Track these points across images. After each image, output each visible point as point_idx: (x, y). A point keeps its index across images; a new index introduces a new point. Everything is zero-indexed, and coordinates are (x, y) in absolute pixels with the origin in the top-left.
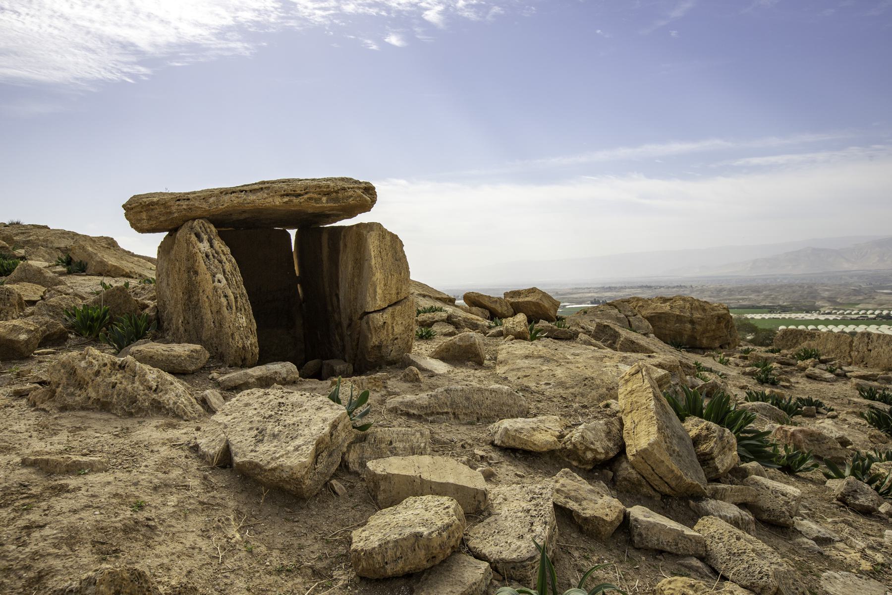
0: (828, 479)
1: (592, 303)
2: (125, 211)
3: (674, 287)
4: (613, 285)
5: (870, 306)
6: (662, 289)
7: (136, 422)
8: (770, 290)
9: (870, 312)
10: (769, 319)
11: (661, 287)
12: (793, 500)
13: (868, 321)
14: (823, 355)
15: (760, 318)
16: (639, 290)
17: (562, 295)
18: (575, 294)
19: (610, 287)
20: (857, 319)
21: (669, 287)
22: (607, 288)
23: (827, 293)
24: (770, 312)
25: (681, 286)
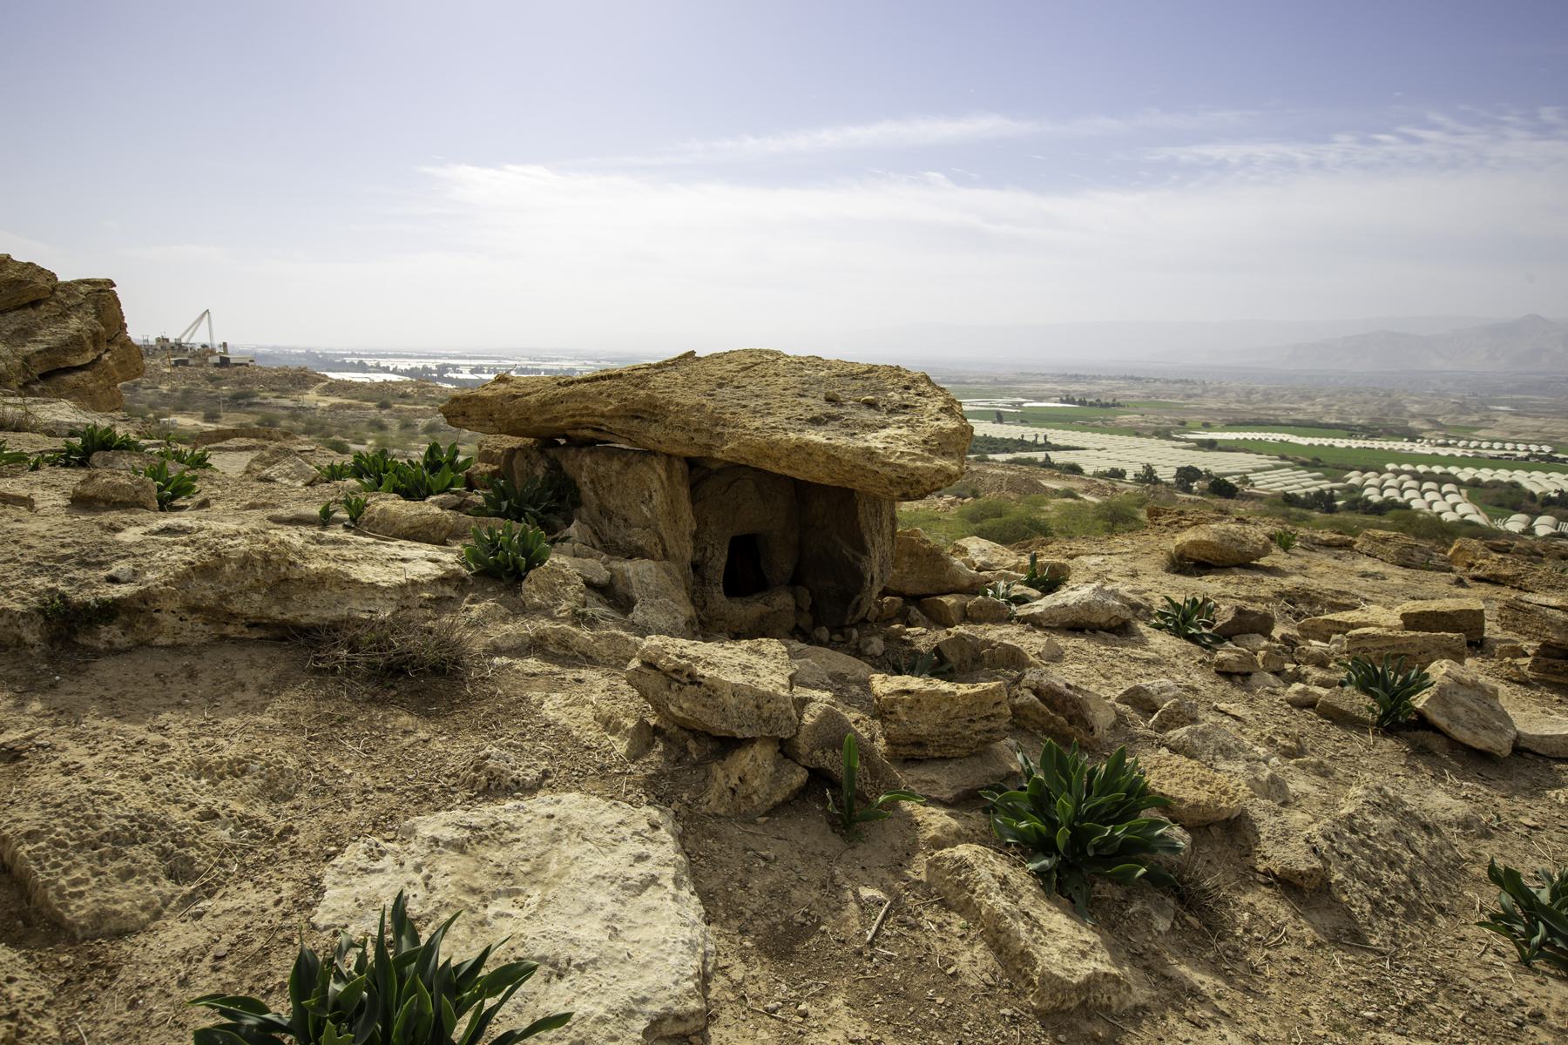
0: (643, 637)
1: (1062, 401)
2: (172, 340)
3: (1176, 382)
4: (1083, 373)
5: (1497, 435)
6: (1158, 384)
7: (286, 980)
8: (1327, 396)
9: (1485, 445)
10: (1359, 448)
11: (1156, 380)
12: (1008, 845)
13: (1510, 462)
14: (395, 447)
15: (1343, 446)
16: (1122, 383)
17: (1006, 383)
18: (1024, 383)
19: (1076, 376)
20: (1499, 458)
21: (1167, 382)
22: (1071, 376)
23: (1417, 406)
24: (1350, 436)
25: (1186, 381)
